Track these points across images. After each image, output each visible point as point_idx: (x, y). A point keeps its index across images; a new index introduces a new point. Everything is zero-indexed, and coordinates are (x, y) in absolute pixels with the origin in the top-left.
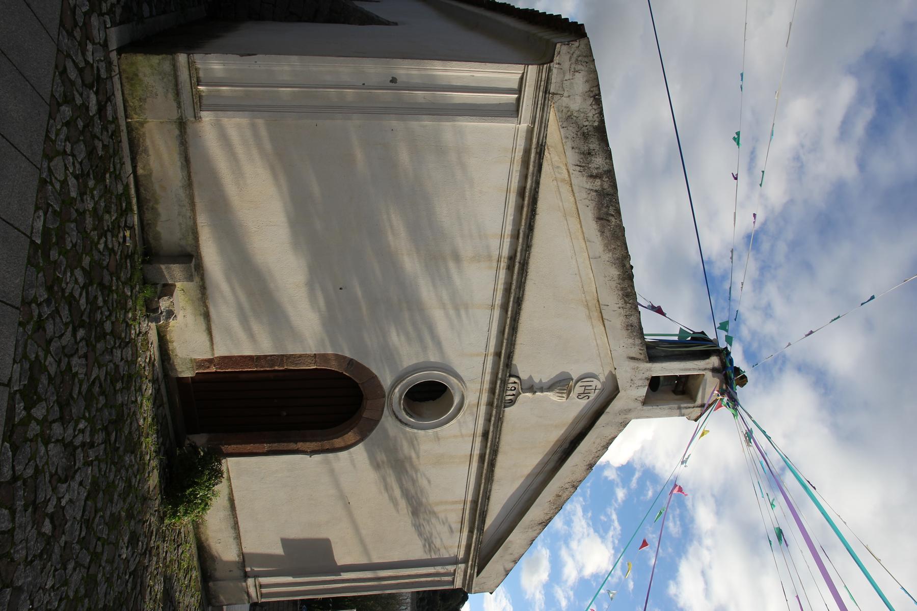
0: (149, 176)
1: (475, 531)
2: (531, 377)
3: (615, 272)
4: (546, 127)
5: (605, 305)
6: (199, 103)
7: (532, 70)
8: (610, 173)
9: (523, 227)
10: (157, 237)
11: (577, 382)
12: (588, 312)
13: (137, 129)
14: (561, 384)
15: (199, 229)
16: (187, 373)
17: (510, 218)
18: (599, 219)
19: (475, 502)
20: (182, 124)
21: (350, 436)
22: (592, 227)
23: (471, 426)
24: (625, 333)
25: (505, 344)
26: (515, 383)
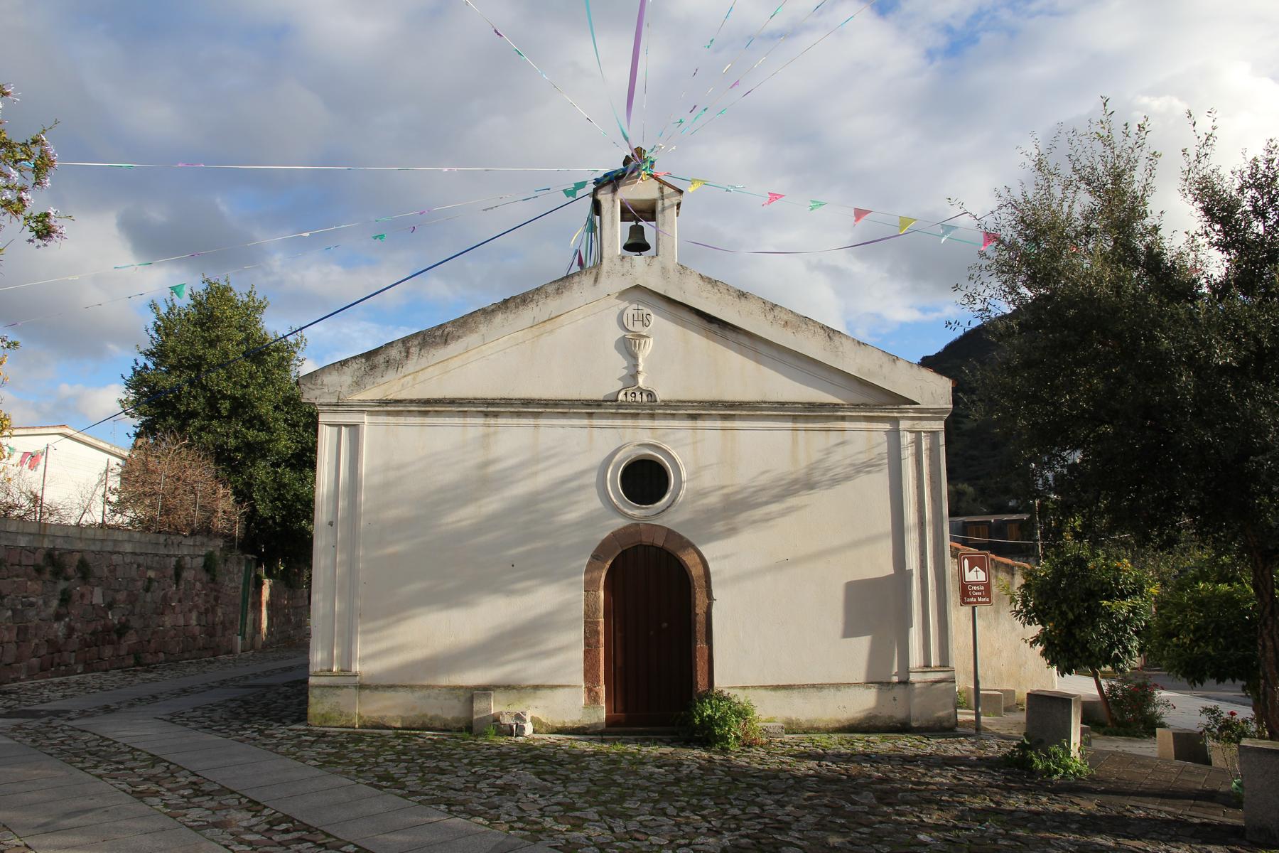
0: (403, 719)
1: (839, 414)
3: (499, 318)
4: (364, 401)
6: (345, 672)
7: (322, 418)
8: (405, 341)
9: (453, 409)
10: (457, 720)
11: (628, 330)
13: (364, 722)
15: (451, 684)
16: (600, 714)
17: (448, 420)
18: (446, 342)
19: (795, 419)
20: (362, 687)
21: (689, 559)
22: (454, 348)
23: (682, 434)
24: (566, 294)
25: (575, 411)
26: (626, 394)
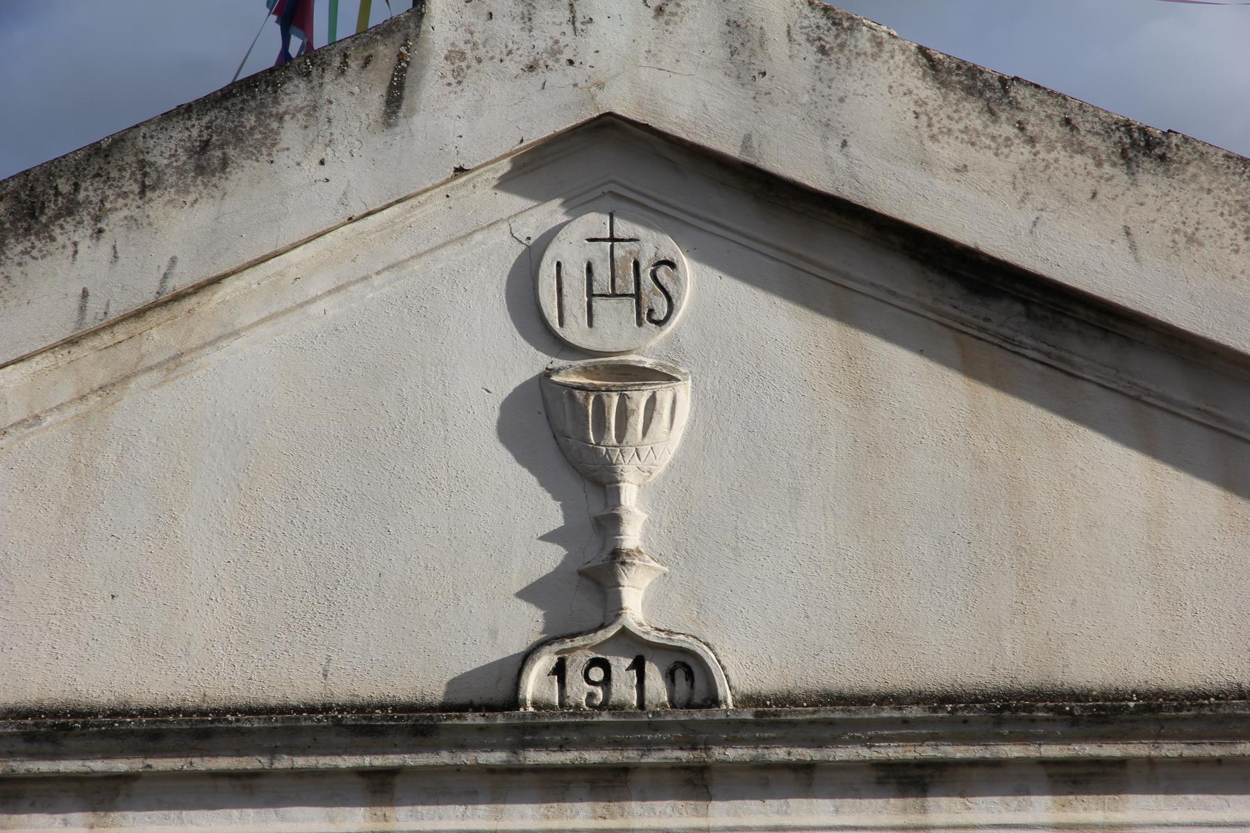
2: (529, 594)
5: (82, 309)
12: (144, 379)
14: (569, 427)
25: (300, 762)
